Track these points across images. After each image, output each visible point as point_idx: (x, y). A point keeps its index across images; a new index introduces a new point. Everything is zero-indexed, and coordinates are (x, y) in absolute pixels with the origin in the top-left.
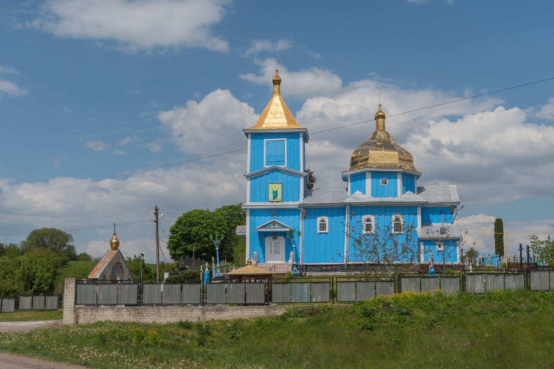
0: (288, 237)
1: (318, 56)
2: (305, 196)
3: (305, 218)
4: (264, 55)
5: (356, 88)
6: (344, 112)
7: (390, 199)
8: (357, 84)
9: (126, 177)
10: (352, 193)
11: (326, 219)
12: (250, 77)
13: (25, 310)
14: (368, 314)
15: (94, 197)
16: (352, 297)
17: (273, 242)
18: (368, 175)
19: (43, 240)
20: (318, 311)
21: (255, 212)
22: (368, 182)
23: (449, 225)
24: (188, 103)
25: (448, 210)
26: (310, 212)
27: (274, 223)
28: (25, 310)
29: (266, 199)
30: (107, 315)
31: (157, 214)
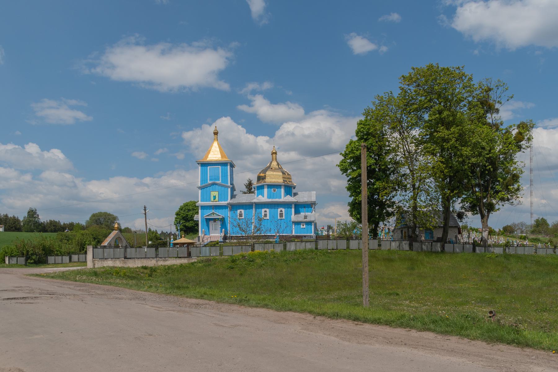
0: (223, 221)
1: (290, 93)
2: (231, 198)
3: (231, 210)
4: (254, 93)
5: (315, 116)
6: (307, 132)
7: (277, 200)
8: (316, 113)
9: (160, 177)
10: (258, 196)
11: (243, 211)
12: (244, 108)
13: (75, 262)
14: (234, 261)
15: (139, 190)
16: (230, 253)
17: (214, 223)
18: (266, 187)
19: (99, 219)
20: (210, 260)
21: (203, 207)
22: (266, 190)
23: (309, 214)
24: (203, 126)
25: (310, 205)
26: (233, 207)
27: (213, 213)
28: (75, 262)
29: (210, 200)
30: (109, 263)
31: (145, 210)
